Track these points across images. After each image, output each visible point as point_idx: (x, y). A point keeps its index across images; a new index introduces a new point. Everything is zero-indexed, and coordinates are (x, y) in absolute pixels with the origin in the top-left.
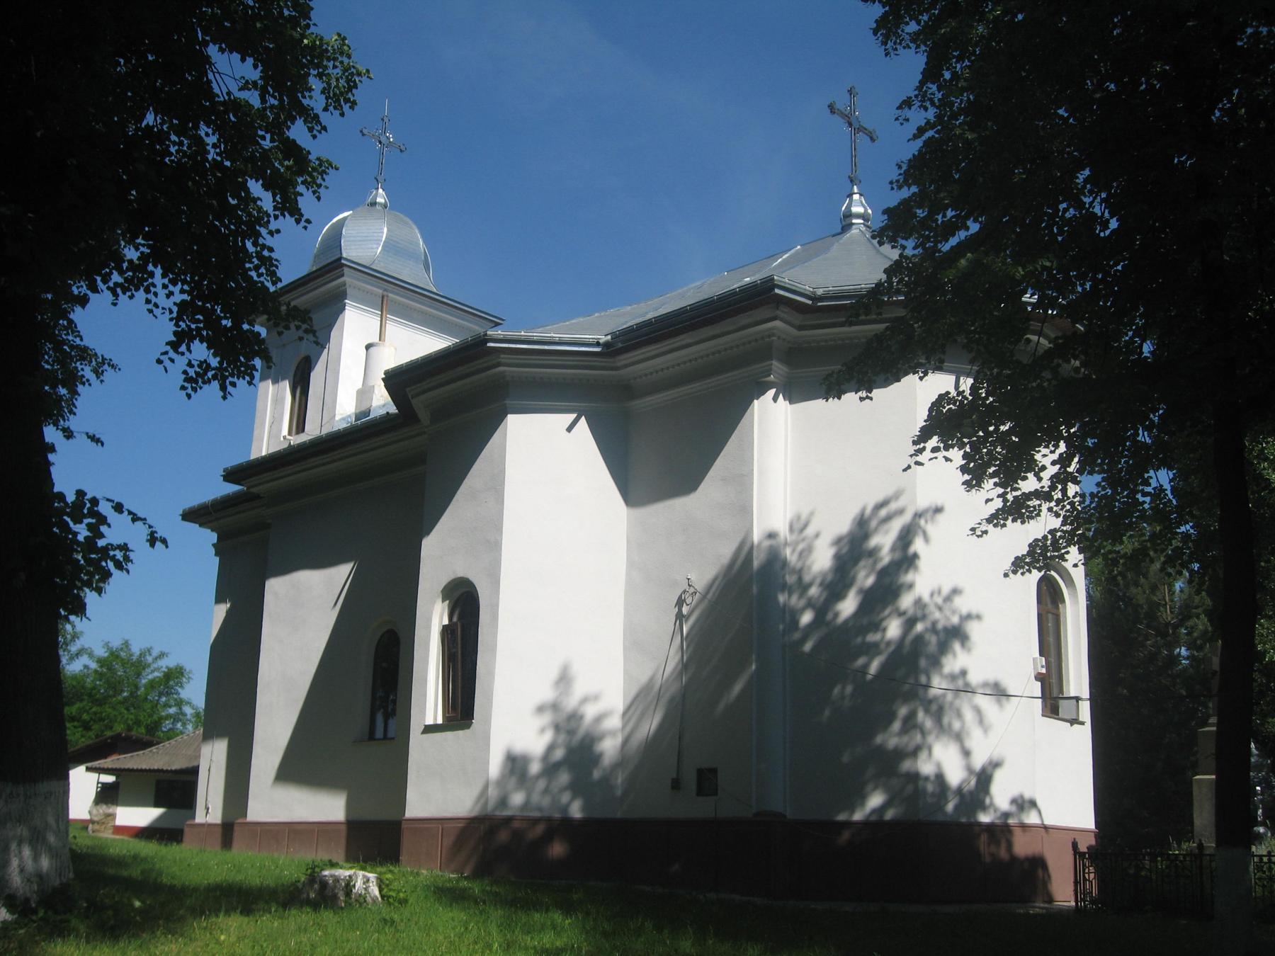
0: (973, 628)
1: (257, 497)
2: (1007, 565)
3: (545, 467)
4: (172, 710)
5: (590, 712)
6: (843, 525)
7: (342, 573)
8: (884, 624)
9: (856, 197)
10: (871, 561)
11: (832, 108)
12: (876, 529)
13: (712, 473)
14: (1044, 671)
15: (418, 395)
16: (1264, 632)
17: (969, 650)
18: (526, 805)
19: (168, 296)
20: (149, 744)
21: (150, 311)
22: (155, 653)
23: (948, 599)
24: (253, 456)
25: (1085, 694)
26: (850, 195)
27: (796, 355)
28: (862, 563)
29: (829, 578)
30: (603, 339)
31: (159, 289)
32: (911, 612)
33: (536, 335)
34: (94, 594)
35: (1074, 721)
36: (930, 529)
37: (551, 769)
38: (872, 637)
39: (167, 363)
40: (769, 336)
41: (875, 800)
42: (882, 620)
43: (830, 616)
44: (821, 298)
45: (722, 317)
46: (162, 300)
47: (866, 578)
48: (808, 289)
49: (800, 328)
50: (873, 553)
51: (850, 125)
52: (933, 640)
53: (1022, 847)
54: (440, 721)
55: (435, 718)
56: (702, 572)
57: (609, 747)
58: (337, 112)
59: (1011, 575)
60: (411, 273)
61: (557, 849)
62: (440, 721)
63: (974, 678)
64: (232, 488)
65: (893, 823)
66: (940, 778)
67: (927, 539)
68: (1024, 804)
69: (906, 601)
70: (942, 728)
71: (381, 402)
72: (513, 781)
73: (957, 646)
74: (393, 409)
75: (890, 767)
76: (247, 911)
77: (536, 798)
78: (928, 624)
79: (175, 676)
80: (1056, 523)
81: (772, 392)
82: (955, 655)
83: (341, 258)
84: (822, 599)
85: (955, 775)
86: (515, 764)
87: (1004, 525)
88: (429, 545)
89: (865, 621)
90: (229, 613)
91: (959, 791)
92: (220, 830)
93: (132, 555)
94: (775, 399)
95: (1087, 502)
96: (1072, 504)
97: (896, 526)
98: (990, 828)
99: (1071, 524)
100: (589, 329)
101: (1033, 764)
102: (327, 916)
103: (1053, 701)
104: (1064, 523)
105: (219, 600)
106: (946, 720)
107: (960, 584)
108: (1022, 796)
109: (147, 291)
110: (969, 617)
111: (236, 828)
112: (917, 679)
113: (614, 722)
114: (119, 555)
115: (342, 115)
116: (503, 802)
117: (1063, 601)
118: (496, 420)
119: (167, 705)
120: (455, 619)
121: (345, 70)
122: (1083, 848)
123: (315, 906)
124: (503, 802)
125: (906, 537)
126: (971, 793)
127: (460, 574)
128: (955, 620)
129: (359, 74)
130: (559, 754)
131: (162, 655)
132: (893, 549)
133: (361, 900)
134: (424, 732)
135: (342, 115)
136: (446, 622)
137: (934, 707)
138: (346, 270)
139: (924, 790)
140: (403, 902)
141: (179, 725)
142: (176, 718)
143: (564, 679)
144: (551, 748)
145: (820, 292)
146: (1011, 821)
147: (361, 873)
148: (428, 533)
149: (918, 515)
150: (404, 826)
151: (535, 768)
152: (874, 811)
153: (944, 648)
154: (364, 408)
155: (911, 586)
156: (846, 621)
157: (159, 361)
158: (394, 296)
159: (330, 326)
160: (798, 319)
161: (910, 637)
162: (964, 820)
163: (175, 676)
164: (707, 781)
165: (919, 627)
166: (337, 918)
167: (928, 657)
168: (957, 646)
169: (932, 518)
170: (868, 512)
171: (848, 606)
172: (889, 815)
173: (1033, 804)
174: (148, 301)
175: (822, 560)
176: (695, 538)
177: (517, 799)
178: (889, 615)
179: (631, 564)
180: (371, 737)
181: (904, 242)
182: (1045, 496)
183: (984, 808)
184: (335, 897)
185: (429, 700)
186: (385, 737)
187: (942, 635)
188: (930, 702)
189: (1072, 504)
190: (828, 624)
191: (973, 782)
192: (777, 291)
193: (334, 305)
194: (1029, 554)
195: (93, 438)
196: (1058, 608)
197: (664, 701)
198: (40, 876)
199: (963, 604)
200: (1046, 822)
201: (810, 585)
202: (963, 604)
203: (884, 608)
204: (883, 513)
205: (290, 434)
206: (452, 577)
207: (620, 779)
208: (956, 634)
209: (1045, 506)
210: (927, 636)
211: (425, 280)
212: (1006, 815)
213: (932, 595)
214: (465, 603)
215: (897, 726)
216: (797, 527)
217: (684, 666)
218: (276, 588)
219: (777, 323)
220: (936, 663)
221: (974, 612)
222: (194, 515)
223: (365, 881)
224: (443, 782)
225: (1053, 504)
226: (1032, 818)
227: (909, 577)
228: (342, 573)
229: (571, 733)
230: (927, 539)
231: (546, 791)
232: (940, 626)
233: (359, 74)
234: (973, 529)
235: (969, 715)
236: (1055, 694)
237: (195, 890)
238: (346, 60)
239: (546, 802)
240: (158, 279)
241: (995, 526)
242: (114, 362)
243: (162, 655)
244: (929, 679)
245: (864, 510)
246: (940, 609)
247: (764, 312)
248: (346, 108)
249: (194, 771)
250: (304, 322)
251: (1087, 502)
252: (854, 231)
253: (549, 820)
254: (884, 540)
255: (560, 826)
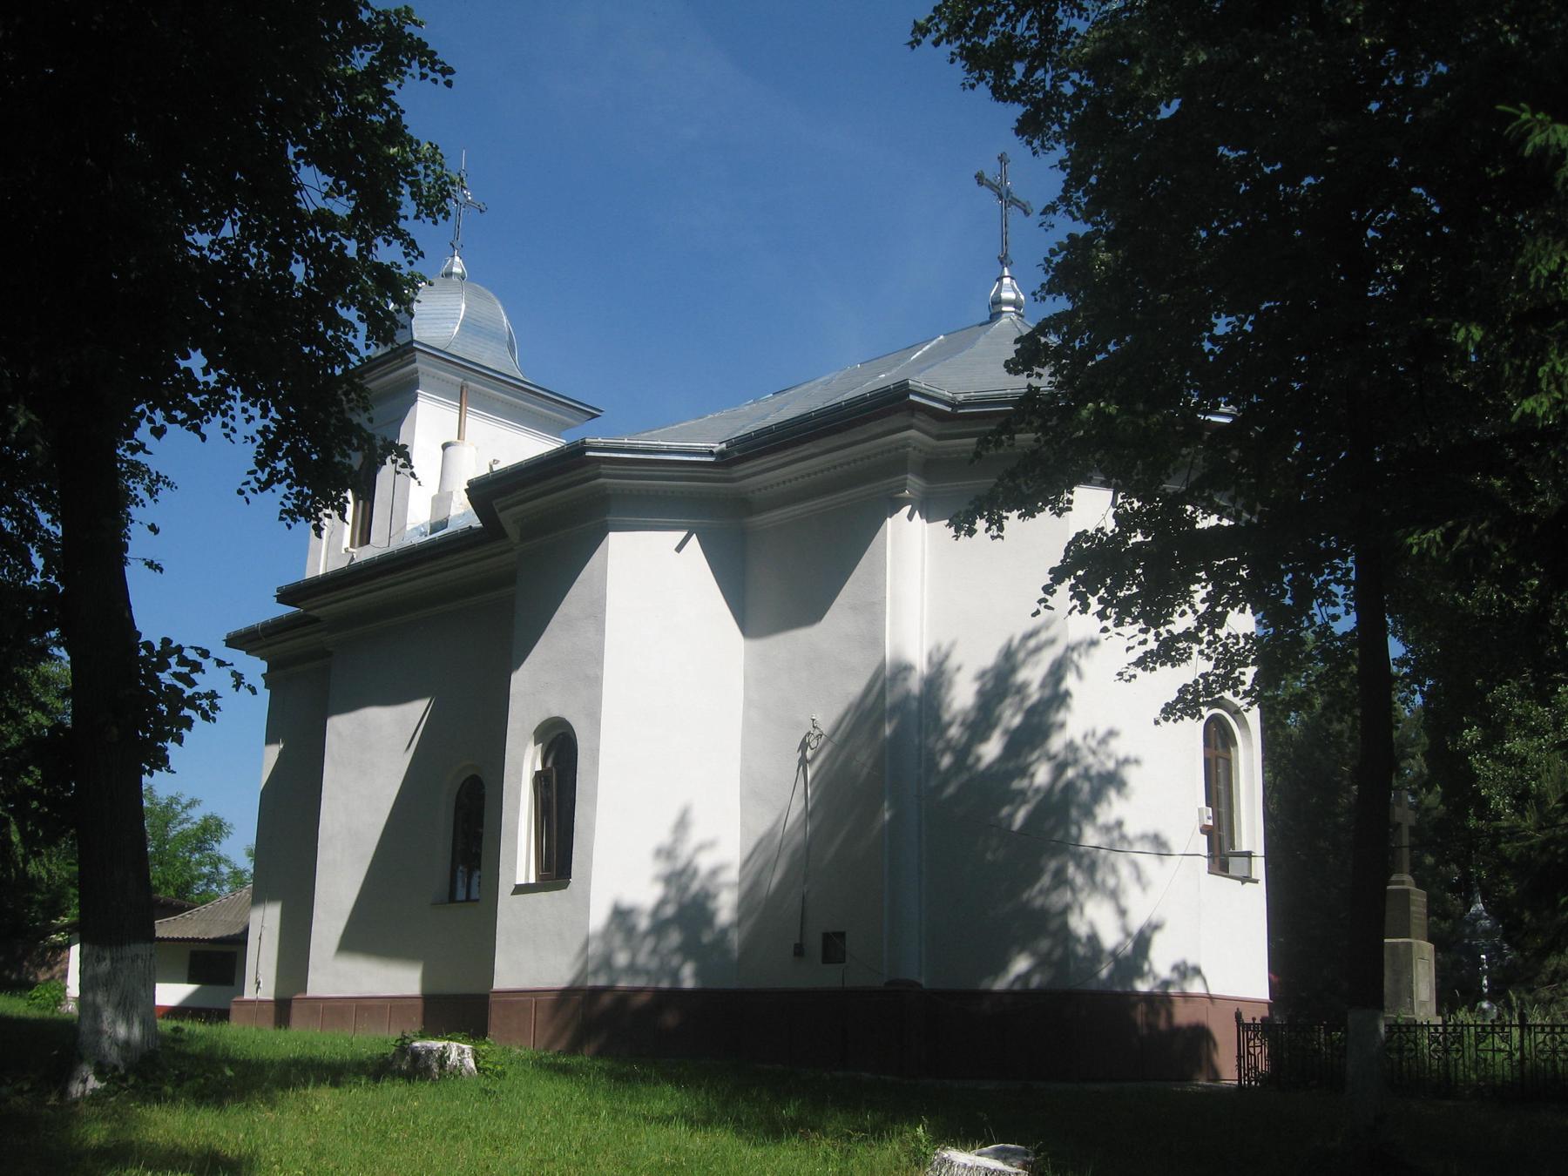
0: (1131, 774)
1: (316, 620)
2: (1157, 714)
3: (651, 596)
4: (206, 870)
5: (705, 862)
6: (986, 656)
7: (415, 712)
8: (1032, 769)
9: (1006, 281)
10: (1018, 698)
11: (980, 179)
12: (1024, 662)
13: (841, 599)
14: (1210, 823)
15: (507, 507)
16: (1491, 774)
17: (1127, 798)
18: (632, 969)
19: (248, 421)
20: (179, 910)
21: (227, 436)
22: (184, 801)
23: (1103, 741)
24: (309, 575)
25: (1259, 850)
26: (1000, 279)
27: (932, 467)
28: (1008, 701)
29: (972, 716)
30: (718, 447)
31: (237, 412)
32: (1061, 757)
33: (640, 442)
34: (175, 744)
35: (1246, 879)
36: (1084, 663)
37: (660, 927)
38: (1019, 784)
39: (249, 494)
40: (904, 447)
41: (1021, 964)
42: (1030, 764)
43: (971, 760)
44: (962, 405)
45: (850, 426)
46: (240, 423)
47: (1012, 718)
48: (947, 394)
49: (939, 437)
50: (1022, 689)
51: (1001, 197)
52: (1086, 787)
53: (1183, 1015)
54: (532, 880)
55: (527, 877)
56: (827, 713)
57: (726, 908)
58: (429, 221)
59: (1162, 722)
60: (492, 356)
61: (670, 1019)
62: (532, 880)
63: (1131, 829)
64: (286, 610)
65: (1039, 992)
66: (1093, 939)
67: (1080, 675)
68: (1186, 971)
69: (1056, 743)
70: (1095, 886)
71: (462, 513)
72: (618, 940)
73: (1112, 794)
74: (476, 523)
75: (1049, 928)
76: (335, 1084)
77: (642, 958)
78: (1080, 769)
79: (212, 829)
80: (1208, 666)
81: (907, 509)
82: (1110, 804)
83: (412, 341)
84: (964, 739)
85: (1111, 937)
86: (621, 916)
87: (1154, 669)
88: (520, 681)
89: (1011, 765)
90: (281, 754)
91: (1114, 953)
92: (272, 1007)
93: (217, 701)
94: (910, 517)
95: (1242, 644)
96: (1225, 645)
97: (1048, 657)
98: (1149, 997)
99: (1225, 667)
100: (700, 434)
101: (1193, 918)
102: (424, 1089)
103: (1221, 854)
104: (1216, 667)
105: (270, 739)
106: (1099, 877)
107: (1117, 726)
108: (1184, 963)
109: (224, 414)
110: (1126, 761)
111: (294, 1004)
112: (1067, 832)
113: (732, 875)
114: (205, 703)
115: (435, 223)
116: (607, 963)
117: (1235, 744)
118: (595, 539)
119: (200, 863)
120: (549, 765)
121: (438, 178)
122: (1247, 1019)
123: (409, 1077)
124: (607, 963)
125: (1057, 671)
126: (1127, 958)
127: (555, 714)
128: (1111, 765)
129: (453, 183)
130: (670, 910)
131: (192, 804)
132: (1043, 685)
133: (457, 1072)
134: (514, 893)
135: (435, 223)
136: (539, 767)
137: (1086, 861)
138: (418, 354)
139: (1074, 954)
140: (501, 1075)
141: (214, 886)
142: (210, 879)
143: (682, 824)
144: (662, 903)
145: (961, 397)
146: (1172, 991)
147: (454, 1045)
148: (518, 667)
149: (1071, 648)
150: (492, 999)
151: (644, 923)
152: (1019, 978)
153: (1097, 796)
154: (440, 518)
155: (1062, 725)
156: (990, 767)
157: (241, 492)
158: (476, 386)
159: (400, 420)
160: (936, 427)
161: (1060, 784)
162: (1119, 989)
163: (212, 829)
164: (833, 947)
165: (1070, 773)
166: (433, 1089)
167: (1079, 806)
168: (1112, 794)
169: (1087, 652)
170: (1016, 642)
171: (991, 750)
172: (1035, 982)
173: (1197, 971)
174: (225, 425)
175: (962, 696)
176: (821, 672)
177: (622, 959)
178: (1038, 759)
179: (748, 703)
180: (452, 898)
181: (1040, 370)
182: (1191, 636)
183: (1141, 974)
184: (428, 1068)
185: (520, 855)
186: (468, 899)
187: (1095, 782)
188: (1081, 856)
189: (1225, 645)
190: (970, 768)
191: (1130, 945)
192: (912, 397)
193: (405, 395)
194: (1178, 700)
195: (150, 564)
196: (1229, 752)
197: (788, 852)
198: (127, 1044)
199: (1119, 748)
200: (1212, 992)
201: (950, 724)
202: (1119, 748)
203: (1033, 749)
204: (1032, 643)
205: (352, 545)
206: (546, 717)
207: (735, 939)
208: (1111, 781)
209: (1196, 648)
210: (1079, 783)
211: (508, 365)
212: (1166, 984)
213: (1085, 737)
214: (560, 744)
215: (1046, 880)
216: (935, 659)
217: (809, 814)
218: (341, 729)
219: (912, 433)
220: (1089, 814)
221: (1132, 755)
222: (241, 640)
223: (459, 1052)
224: (534, 950)
225: (1204, 646)
226: (1195, 987)
227: (1061, 716)
228: (415, 712)
229: (684, 889)
230: (1080, 675)
231: (654, 951)
232: (1093, 772)
233: (453, 183)
234: (1120, 674)
235: (1125, 871)
236: (1226, 850)
237: (272, 1063)
238: (438, 169)
239: (654, 964)
240: (238, 406)
241: (1144, 669)
242: (170, 479)
243: (192, 804)
244: (1080, 830)
245: (1011, 640)
246: (1094, 753)
247: (897, 420)
248: (439, 218)
249: (240, 940)
250: (399, 456)
251: (1242, 644)
252: (1004, 320)
253: (658, 992)
254: (1033, 674)
255: (673, 997)
